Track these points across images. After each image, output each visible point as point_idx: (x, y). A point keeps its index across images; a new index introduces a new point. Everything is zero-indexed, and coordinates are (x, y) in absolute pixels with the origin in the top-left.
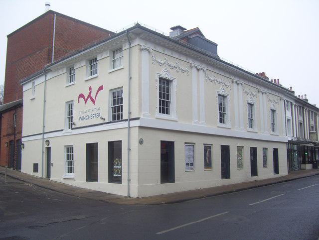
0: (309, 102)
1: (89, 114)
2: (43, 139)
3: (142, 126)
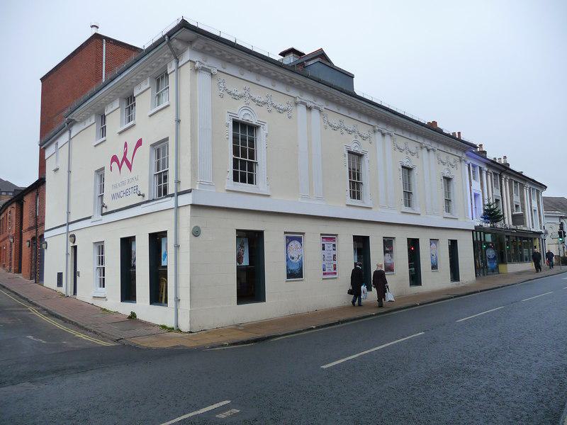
0: (511, 167)
1: (124, 188)
2: (68, 232)
3: (195, 203)
